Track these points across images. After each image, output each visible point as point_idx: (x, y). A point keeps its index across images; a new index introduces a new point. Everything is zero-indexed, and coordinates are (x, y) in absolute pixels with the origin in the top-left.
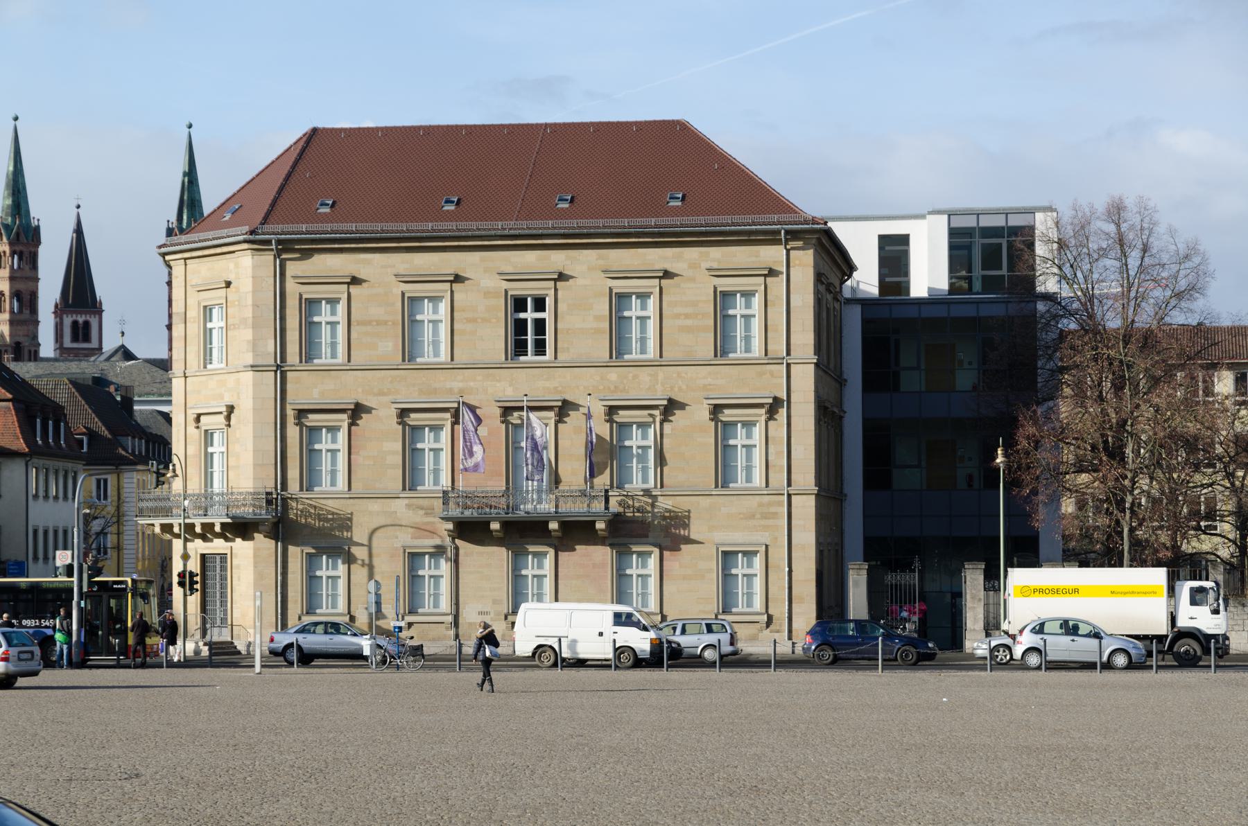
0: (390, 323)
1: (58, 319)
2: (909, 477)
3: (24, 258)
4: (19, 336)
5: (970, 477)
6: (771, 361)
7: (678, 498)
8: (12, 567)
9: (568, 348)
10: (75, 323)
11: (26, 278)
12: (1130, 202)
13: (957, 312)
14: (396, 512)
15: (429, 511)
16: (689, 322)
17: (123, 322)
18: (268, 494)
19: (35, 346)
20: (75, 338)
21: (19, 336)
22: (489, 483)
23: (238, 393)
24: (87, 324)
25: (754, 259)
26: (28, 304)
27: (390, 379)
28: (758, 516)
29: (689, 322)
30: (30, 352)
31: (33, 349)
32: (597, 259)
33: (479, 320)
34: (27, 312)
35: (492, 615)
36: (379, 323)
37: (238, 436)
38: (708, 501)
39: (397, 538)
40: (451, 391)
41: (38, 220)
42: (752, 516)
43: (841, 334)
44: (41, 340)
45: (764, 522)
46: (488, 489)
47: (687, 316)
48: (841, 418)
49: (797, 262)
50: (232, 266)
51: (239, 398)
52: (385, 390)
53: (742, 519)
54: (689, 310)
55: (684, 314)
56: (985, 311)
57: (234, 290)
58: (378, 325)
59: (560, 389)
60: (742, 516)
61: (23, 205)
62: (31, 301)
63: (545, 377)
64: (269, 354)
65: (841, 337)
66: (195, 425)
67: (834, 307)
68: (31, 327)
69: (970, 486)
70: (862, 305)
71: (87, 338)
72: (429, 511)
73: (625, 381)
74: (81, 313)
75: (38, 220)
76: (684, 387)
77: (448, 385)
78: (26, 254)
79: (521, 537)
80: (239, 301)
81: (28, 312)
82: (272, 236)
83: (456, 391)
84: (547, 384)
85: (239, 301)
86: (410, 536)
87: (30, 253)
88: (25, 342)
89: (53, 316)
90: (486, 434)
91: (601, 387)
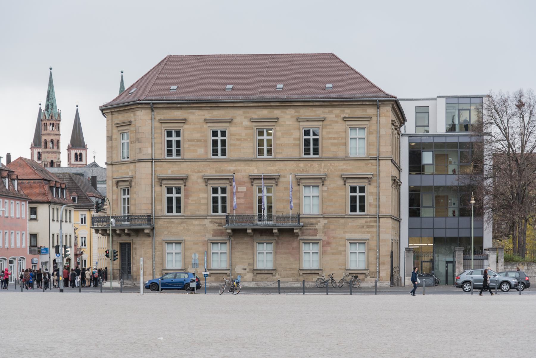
0: (203, 141)
1: (69, 152)
2: (427, 212)
3: (55, 126)
4: (53, 158)
5: (454, 212)
6: (372, 159)
7: (330, 219)
8: (43, 250)
9: (282, 152)
10: (76, 154)
11: (56, 134)
12: (525, 92)
13: (450, 140)
14: (205, 225)
15: (220, 224)
16: (335, 141)
17: (95, 152)
18: (148, 216)
19: (59, 162)
20: (76, 160)
21: (53, 158)
22: (247, 212)
23: (135, 172)
24: (81, 154)
25: (364, 113)
26: (56, 145)
27: (203, 166)
28: (365, 227)
29: (335, 141)
30: (57, 164)
31: (58, 163)
32: (295, 113)
33: (242, 140)
34: (55, 148)
35: (248, 270)
36: (198, 141)
37: (135, 190)
38: (343, 220)
39: (206, 236)
40: (230, 171)
41: (60, 110)
42: (363, 227)
43: (400, 149)
44: (61, 160)
45: (367, 230)
46: (246, 214)
47: (335, 138)
48: (400, 185)
49: (383, 115)
50: (132, 115)
51: (135, 174)
52: (201, 171)
53: (358, 228)
54: (336, 136)
55: (333, 137)
56: (462, 140)
57: (133, 126)
58: (197, 141)
59: (278, 170)
60: (358, 227)
61: (54, 105)
62: (57, 144)
63: (271, 165)
64: (149, 154)
65: (400, 150)
66: (116, 186)
67: (398, 137)
68: (57, 154)
69: (454, 215)
70: (409, 136)
71: (81, 160)
72: (220, 224)
73: (307, 167)
74: (78, 149)
75: (60, 110)
76: (333, 170)
77: (229, 168)
78: (55, 125)
79: (260, 236)
80: (135, 131)
81: (56, 148)
82: (151, 101)
83: (232, 171)
84: (273, 168)
85: (135, 131)
86: (211, 235)
87: (57, 124)
88: (55, 160)
89: (67, 151)
90: (245, 190)
91: (297, 170)
